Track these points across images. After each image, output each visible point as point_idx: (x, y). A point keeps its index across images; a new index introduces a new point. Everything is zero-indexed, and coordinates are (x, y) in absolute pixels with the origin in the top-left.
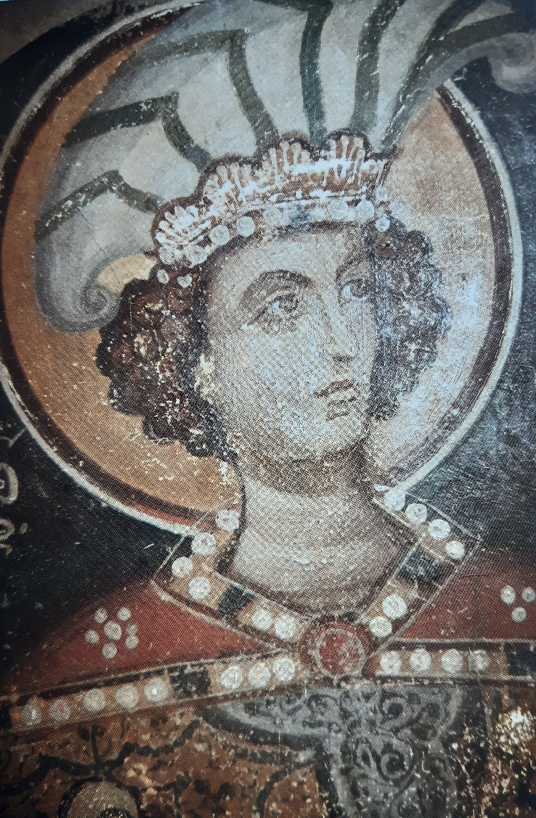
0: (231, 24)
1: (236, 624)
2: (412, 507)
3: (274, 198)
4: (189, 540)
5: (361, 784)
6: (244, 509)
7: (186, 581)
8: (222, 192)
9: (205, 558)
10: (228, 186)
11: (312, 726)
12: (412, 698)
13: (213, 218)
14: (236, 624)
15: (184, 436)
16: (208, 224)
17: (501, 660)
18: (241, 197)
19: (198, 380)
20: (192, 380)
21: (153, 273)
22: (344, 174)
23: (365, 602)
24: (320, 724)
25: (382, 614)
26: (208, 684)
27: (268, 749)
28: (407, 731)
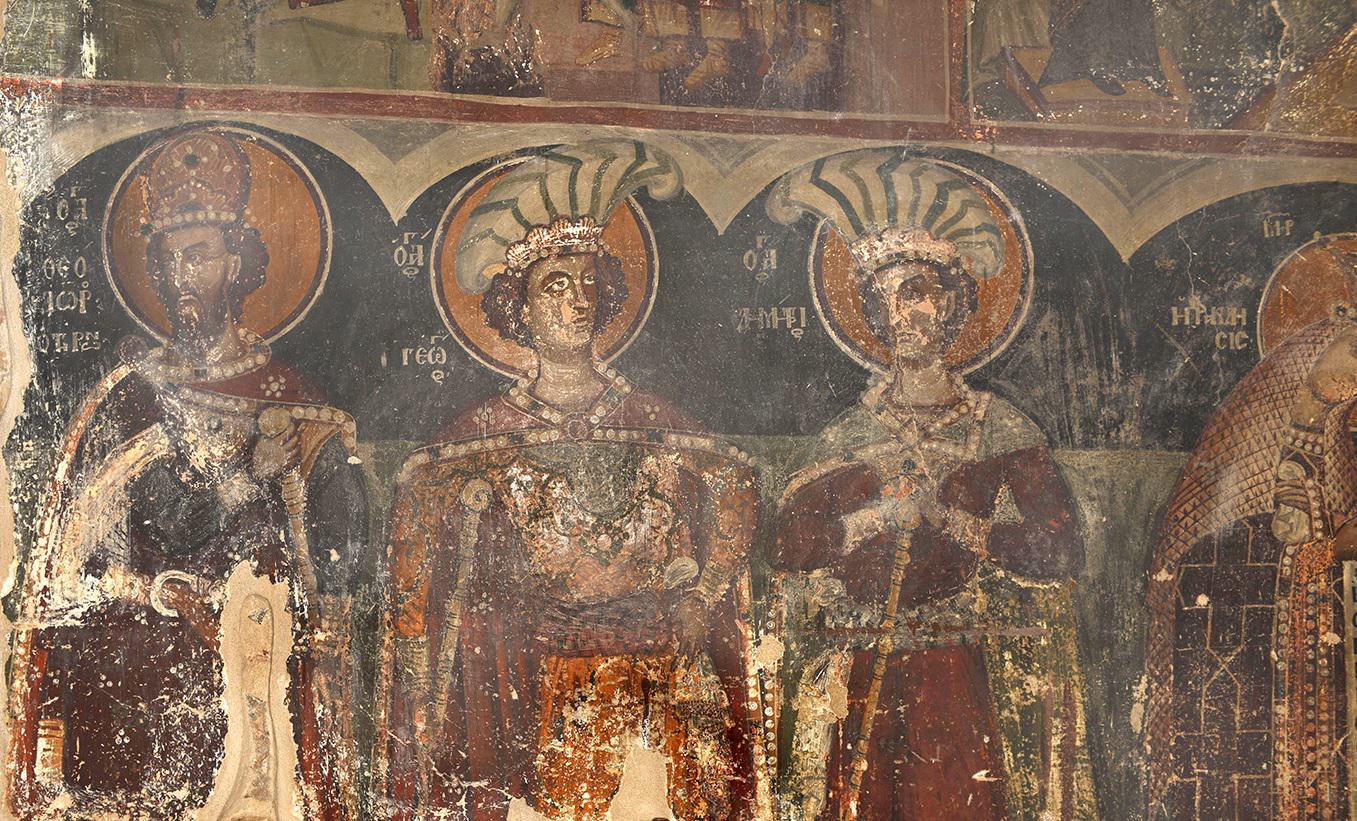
4: (517, 381)
8: (534, 239)
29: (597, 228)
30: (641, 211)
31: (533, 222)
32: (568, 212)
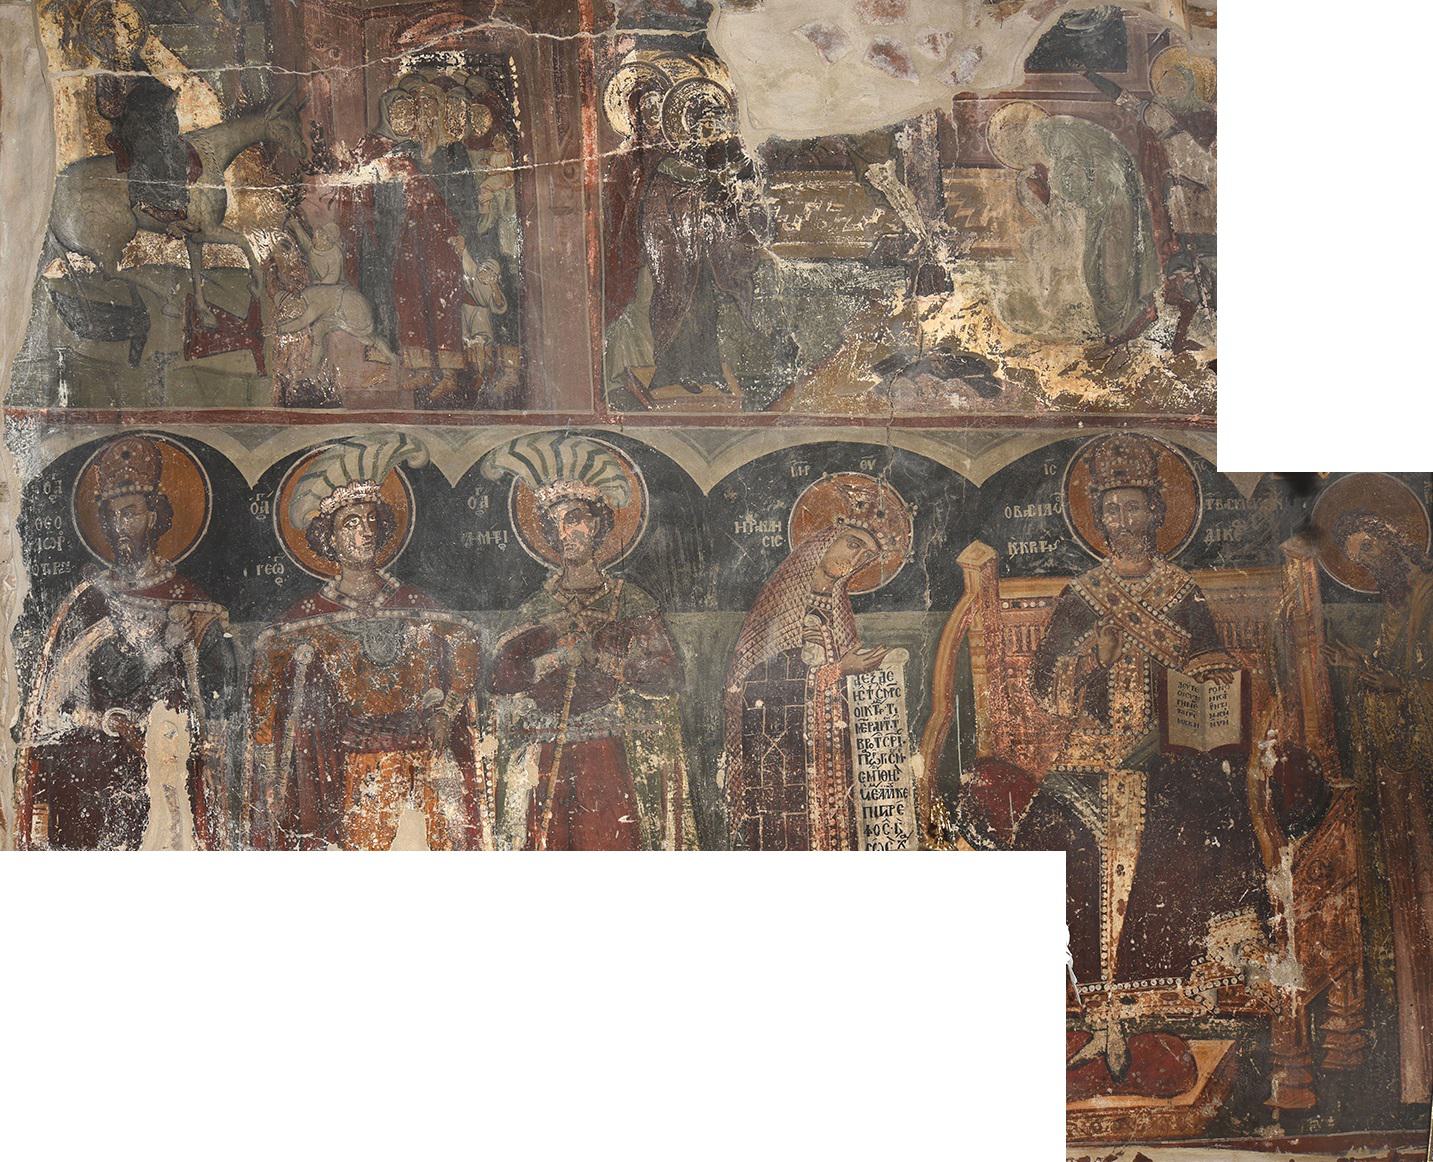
32: (358, 478)
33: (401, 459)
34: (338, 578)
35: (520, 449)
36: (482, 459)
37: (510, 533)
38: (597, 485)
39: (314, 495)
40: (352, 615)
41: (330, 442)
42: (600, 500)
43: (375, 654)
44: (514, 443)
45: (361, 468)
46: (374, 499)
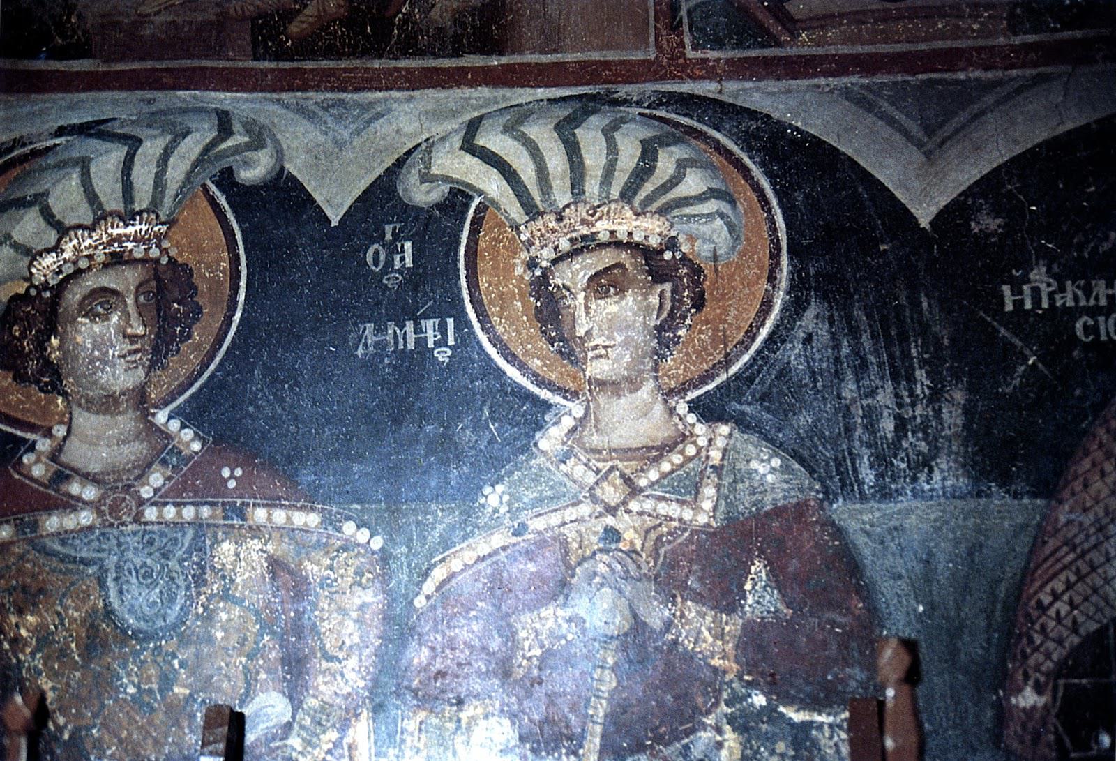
0: (83, 153)
1: (57, 491)
2: (172, 421)
3: (101, 247)
4: (35, 442)
5: (125, 587)
6: (70, 423)
7: (30, 467)
8: (71, 245)
9: (43, 453)
10: (75, 242)
11: (98, 551)
12: (162, 534)
13: (65, 259)
14: (57, 491)
15: (38, 382)
16: (62, 262)
17: (219, 511)
18: (82, 247)
19: (49, 350)
20: (46, 350)
21: (28, 290)
22: (143, 233)
23: (139, 477)
24: (104, 550)
25: (148, 485)
26: (38, 527)
27: (70, 566)
28: (157, 554)
29: (160, 227)
30: (222, 201)
31: (69, 222)
32: (120, 207)
33: (216, 169)
34: (60, 431)
35: (493, 140)
36: (400, 163)
37: (462, 322)
38: (663, 211)
39: (16, 246)
40: (86, 517)
41: (61, 132)
42: (672, 244)
43: (131, 610)
44: (473, 127)
45: (128, 190)
46: (154, 252)
